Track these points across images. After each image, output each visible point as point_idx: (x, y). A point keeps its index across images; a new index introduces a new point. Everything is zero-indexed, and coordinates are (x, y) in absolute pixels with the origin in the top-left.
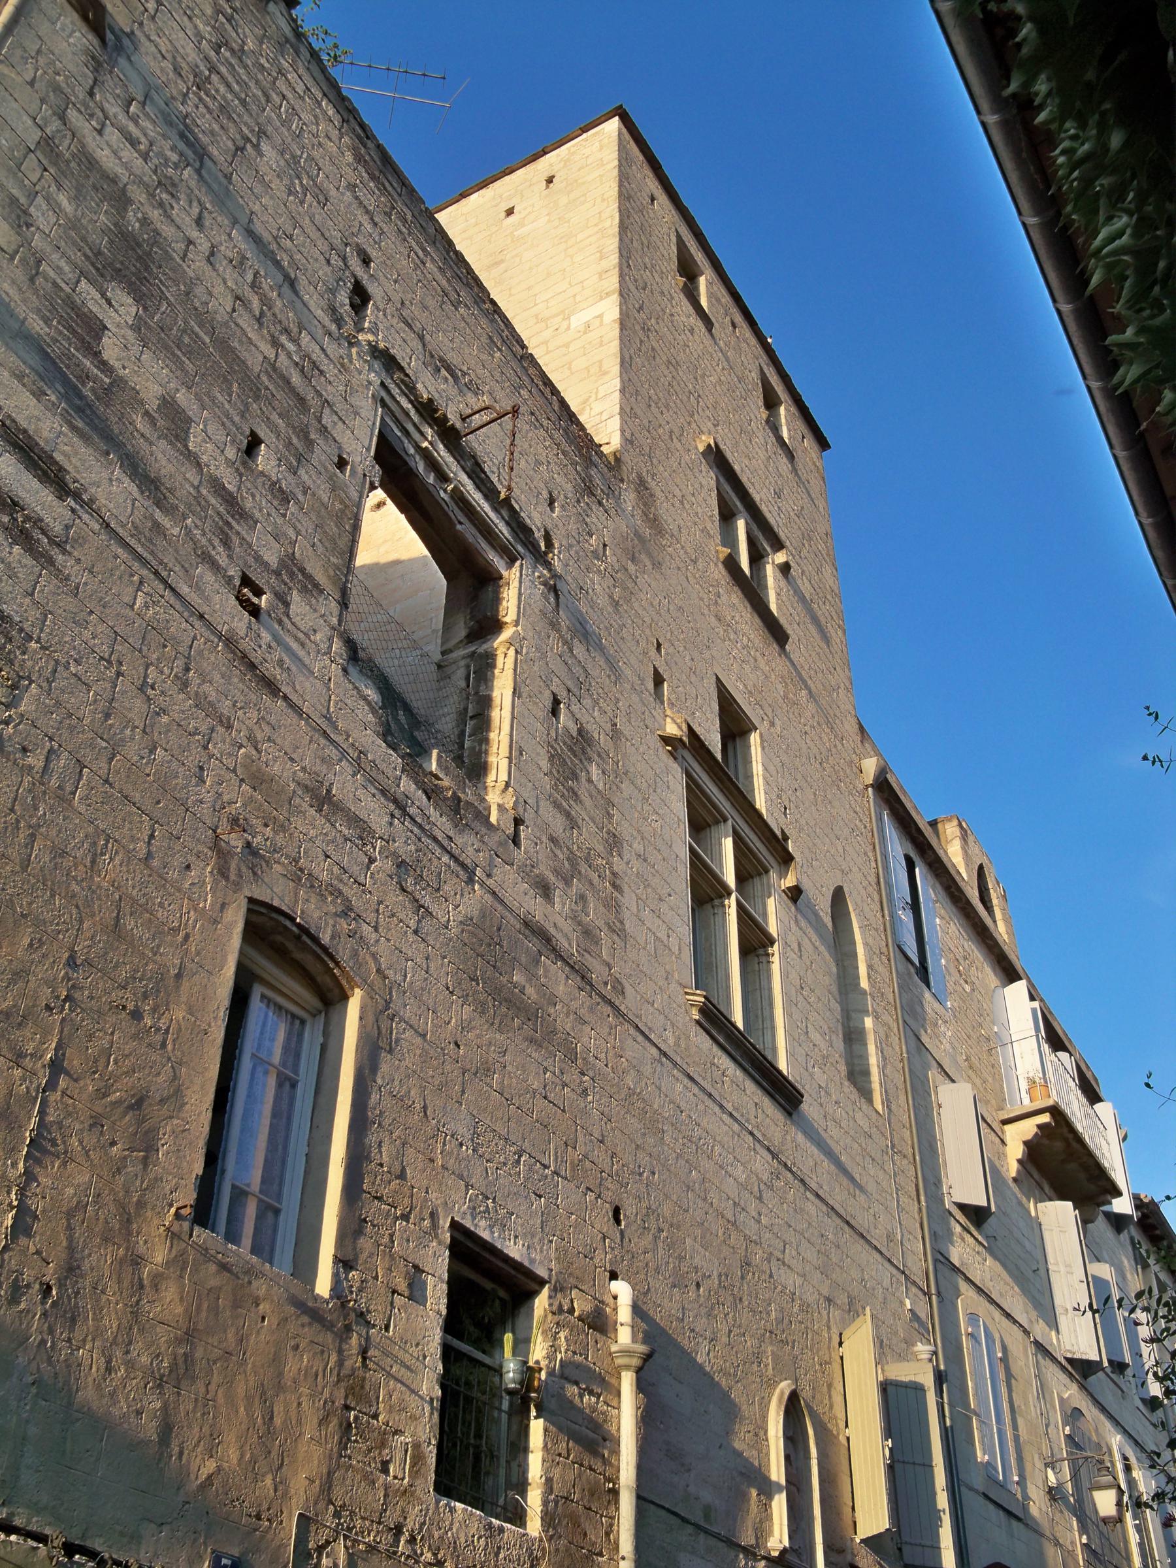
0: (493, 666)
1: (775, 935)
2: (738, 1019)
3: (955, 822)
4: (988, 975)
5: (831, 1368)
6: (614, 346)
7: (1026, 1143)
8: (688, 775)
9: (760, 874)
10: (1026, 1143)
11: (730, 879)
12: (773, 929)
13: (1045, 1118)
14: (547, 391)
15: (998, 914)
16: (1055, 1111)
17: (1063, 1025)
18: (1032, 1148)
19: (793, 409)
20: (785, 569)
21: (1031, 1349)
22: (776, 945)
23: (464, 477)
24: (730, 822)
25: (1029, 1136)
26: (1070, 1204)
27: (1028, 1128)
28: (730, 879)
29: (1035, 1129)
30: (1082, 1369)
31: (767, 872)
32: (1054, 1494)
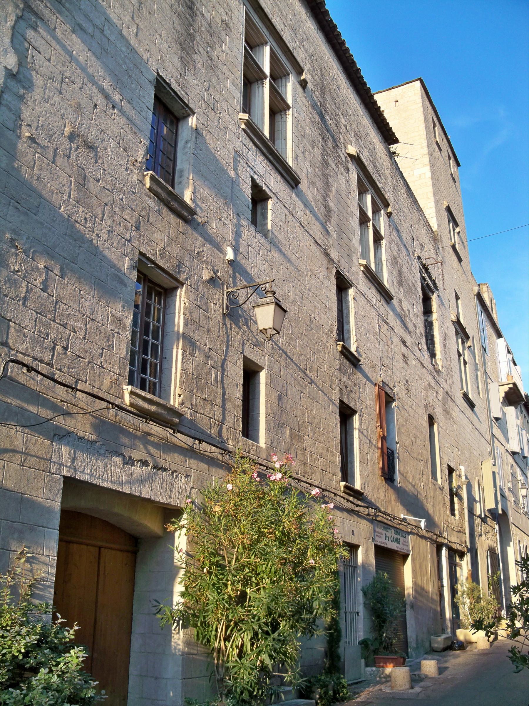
0: (433, 325)
1: (291, 105)
2: (266, 133)
3: (486, 286)
4: (494, 336)
5: (479, 473)
6: (430, 189)
7: (505, 392)
8: (455, 328)
9: (285, 76)
10: (505, 392)
11: (267, 70)
12: (290, 101)
13: (511, 386)
14: (427, 224)
15: (494, 312)
16: (515, 384)
17: (511, 348)
18: (507, 394)
19: (440, 128)
20: (459, 233)
21: (505, 451)
22: (291, 110)
23: (429, 281)
24: (269, 43)
25: (506, 391)
26: (513, 407)
27: (506, 388)
28: (267, 70)
29: (508, 389)
30: (514, 454)
31: (289, 75)
32: (509, 489)
